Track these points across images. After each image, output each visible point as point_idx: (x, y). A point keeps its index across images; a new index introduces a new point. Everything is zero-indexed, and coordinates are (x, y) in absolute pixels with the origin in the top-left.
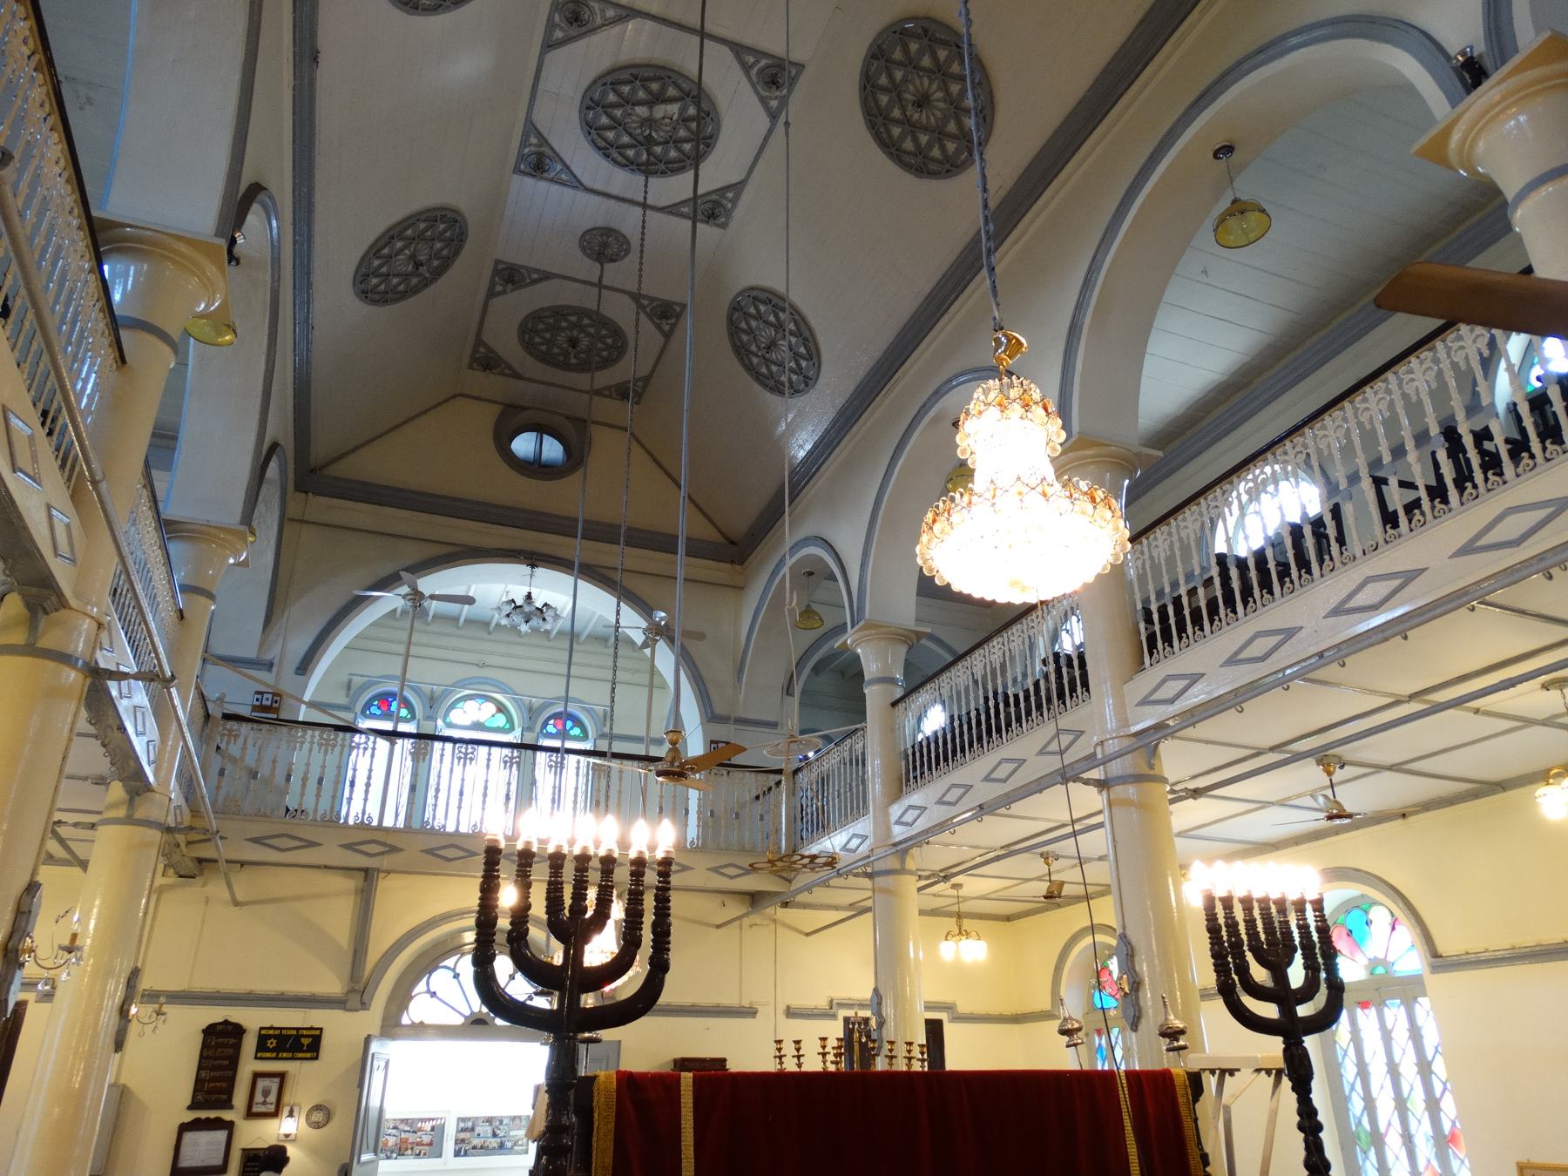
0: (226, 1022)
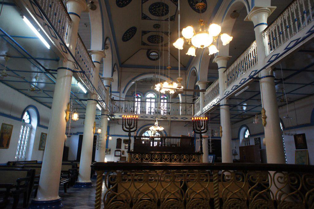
0: (119, 138)
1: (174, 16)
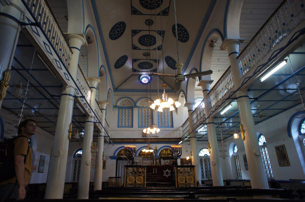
1: (160, 46)
